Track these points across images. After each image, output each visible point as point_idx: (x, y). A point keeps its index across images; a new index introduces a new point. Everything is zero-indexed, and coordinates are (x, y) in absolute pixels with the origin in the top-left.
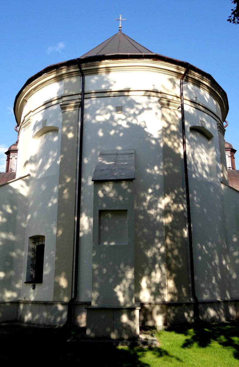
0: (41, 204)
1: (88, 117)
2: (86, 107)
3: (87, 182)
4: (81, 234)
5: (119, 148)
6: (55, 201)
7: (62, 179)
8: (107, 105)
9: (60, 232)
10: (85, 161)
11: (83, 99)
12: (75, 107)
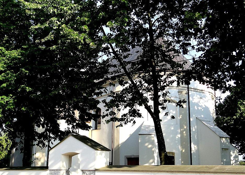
0: (171, 136)
1: (191, 98)
2: (190, 94)
3: (193, 129)
4: (192, 152)
5: (202, 116)
6: (179, 136)
7: (181, 127)
8: (197, 95)
9: (184, 151)
10: (191, 120)
11: (188, 90)
12: (186, 93)
